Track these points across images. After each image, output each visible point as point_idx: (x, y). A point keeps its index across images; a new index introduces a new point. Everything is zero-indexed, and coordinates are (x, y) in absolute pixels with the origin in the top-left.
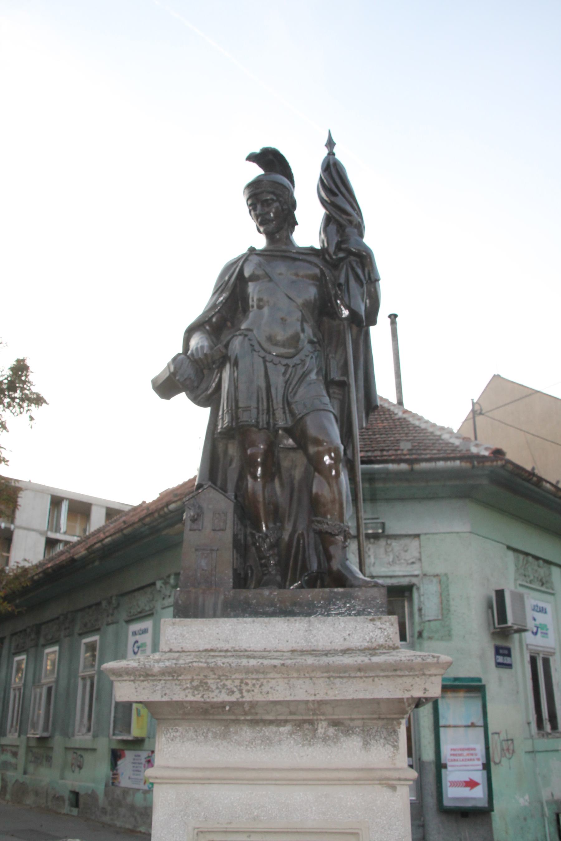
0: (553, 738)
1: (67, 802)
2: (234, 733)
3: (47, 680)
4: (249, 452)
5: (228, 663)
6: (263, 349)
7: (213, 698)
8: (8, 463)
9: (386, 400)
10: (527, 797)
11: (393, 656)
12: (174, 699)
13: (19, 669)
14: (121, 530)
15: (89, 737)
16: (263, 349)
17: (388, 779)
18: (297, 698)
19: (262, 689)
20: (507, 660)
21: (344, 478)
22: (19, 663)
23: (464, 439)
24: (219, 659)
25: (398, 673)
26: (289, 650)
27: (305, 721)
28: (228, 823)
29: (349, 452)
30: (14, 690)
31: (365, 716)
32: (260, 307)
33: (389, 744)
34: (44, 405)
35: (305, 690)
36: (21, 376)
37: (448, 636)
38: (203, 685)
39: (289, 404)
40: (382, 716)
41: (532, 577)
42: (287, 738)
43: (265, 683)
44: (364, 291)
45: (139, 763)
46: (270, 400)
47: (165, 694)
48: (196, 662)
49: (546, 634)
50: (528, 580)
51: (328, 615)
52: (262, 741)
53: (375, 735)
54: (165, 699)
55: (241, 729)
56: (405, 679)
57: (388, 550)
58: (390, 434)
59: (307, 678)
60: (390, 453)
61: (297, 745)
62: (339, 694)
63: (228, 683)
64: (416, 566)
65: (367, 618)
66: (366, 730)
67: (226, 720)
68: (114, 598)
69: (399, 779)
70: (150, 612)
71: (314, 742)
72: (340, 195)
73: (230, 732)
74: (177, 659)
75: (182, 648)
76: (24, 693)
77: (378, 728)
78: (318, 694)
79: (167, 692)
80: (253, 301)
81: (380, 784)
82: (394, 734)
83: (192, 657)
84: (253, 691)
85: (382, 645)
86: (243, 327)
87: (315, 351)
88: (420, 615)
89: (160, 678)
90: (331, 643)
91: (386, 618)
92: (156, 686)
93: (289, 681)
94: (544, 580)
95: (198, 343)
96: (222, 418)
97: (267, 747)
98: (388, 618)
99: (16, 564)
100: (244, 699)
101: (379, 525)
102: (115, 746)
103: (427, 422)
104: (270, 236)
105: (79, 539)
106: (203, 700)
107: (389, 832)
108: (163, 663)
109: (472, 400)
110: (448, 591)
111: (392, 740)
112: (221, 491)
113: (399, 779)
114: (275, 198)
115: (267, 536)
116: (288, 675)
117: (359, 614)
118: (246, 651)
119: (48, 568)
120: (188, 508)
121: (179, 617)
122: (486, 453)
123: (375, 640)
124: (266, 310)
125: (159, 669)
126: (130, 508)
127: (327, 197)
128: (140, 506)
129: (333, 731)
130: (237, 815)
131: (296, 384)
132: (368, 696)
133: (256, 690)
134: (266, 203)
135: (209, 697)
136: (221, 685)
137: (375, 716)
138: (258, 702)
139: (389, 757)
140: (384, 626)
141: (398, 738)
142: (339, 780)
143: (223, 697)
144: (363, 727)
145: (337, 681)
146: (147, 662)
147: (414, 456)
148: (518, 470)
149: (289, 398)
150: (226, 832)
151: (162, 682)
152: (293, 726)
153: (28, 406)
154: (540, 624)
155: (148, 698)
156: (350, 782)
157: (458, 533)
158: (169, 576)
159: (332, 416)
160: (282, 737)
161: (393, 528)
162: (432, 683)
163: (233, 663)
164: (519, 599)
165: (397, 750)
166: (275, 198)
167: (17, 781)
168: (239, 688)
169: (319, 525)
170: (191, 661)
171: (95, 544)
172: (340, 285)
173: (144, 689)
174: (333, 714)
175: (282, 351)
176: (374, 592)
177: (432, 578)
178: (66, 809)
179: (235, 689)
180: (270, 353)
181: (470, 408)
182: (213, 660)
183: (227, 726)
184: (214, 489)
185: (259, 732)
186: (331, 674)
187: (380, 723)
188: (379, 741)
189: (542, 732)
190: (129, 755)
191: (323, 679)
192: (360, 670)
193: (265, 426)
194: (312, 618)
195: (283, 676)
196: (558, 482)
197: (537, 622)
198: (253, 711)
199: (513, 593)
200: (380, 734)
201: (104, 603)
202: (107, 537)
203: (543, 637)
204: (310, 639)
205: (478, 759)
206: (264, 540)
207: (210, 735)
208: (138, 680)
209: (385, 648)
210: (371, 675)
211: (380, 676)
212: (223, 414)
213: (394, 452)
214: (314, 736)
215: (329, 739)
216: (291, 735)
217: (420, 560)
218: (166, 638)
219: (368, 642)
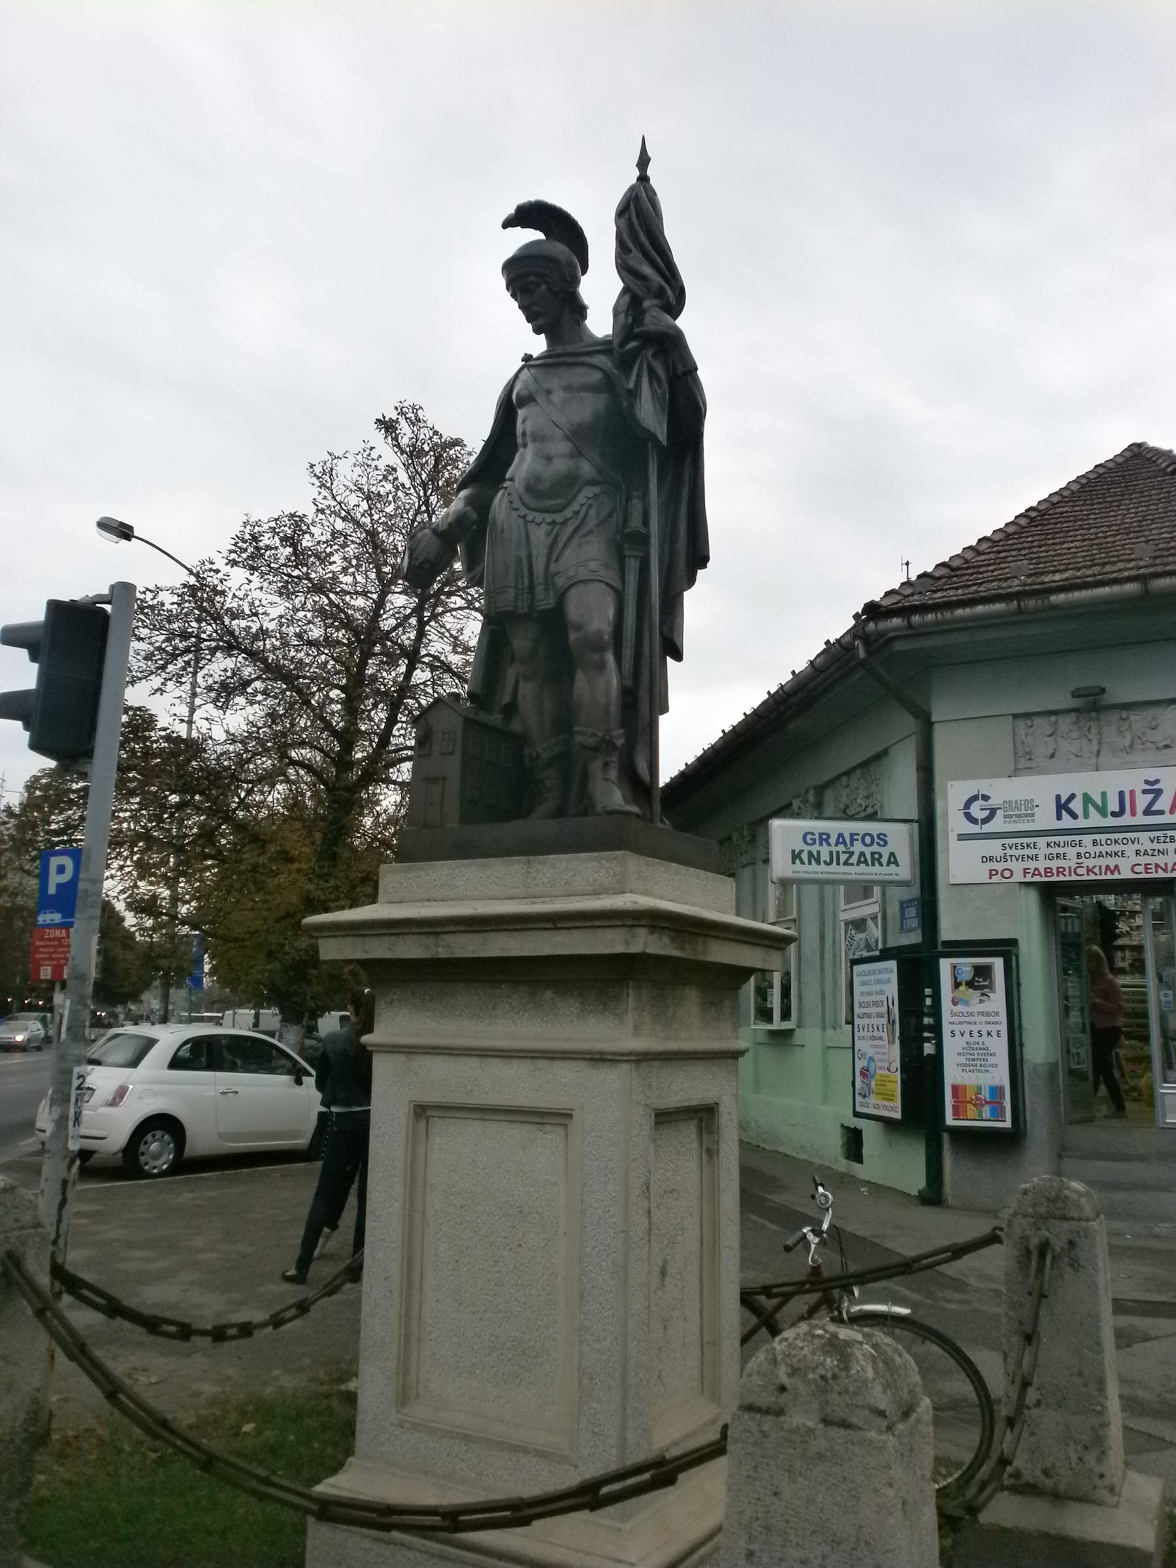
68: (746, 827)
158: (807, 792)
201: (735, 836)
207: (427, 998)
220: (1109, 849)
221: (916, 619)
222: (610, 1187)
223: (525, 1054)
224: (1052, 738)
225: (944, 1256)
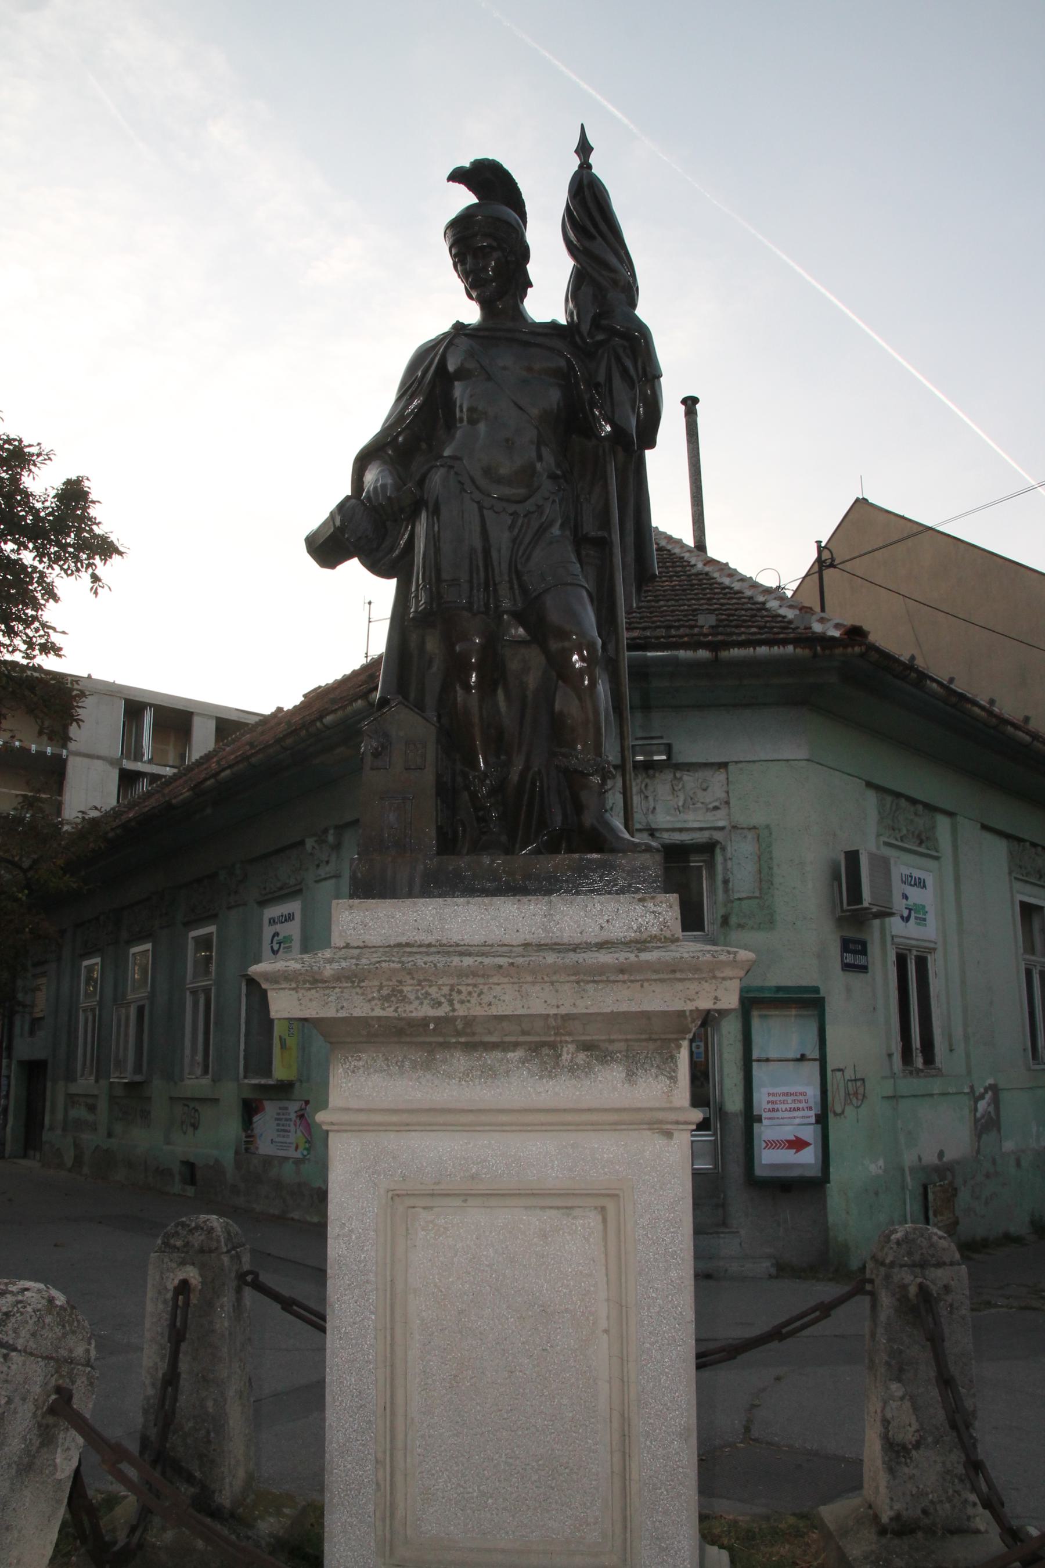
0: (926, 1077)
1: (177, 1178)
2: (441, 1061)
3: (136, 995)
4: (458, 648)
5: (432, 962)
6: (478, 488)
7: (411, 1012)
8: (61, 653)
10: (881, 1163)
11: (672, 951)
12: (355, 1015)
13: (89, 979)
14: (245, 758)
15: (206, 1081)
16: (478, 488)
17: (661, 1122)
18: (532, 1011)
19: (481, 999)
20: (860, 960)
21: (602, 689)
22: (90, 969)
23: (801, 609)
24: (418, 957)
25: (678, 975)
26: (520, 944)
27: (544, 1044)
28: (435, 1183)
29: (611, 653)
30: (85, 1011)
31: (629, 1037)
32: (472, 422)
33: (664, 1075)
34: (115, 557)
36: (76, 508)
37: (769, 922)
38: (397, 995)
39: (519, 575)
40: (654, 1036)
41: (904, 832)
42: (518, 1068)
43: (485, 991)
44: (635, 394)
45: (287, 1120)
46: (490, 569)
47: (342, 1008)
48: (385, 961)
49: (925, 920)
50: (898, 836)
51: (578, 893)
52: (482, 1072)
54: (342, 1014)
56: (687, 984)
57: (676, 788)
58: (683, 599)
59: (546, 982)
60: (682, 631)
61: (532, 1076)
62: (592, 1005)
63: (433, 991)
64: (721, 813)
65: (634, 898)
67: (430, 1043)
69: (677, 1123)
70: (298, 888)
72: (599, 239)
73: (435, 1059)
74: (358, 958)
75: (364, 942)
76: (100, 1015)
80: (461, 411)
81: (649, 1129)
82: (672, 1061)
83: (379, 954)
84: (469, 1001)
85: (656, 936)
86: (446, 453)
87: (559, 490)
88: (726, 890)
89: (334, 985)
90: (581, 933)
91: (662, 897)
92: (329, 996)
94: (924, 837)
95: (377, 480)
96: (417, 597)
98: (665, 897)
99: (80, 815)
100: (456, 1014)
101: (662, 748)
102: (247, 1094)
103: (743, 579)
104: (486, 305)
105: (175, 770)
106: (396, 1015)
107: (661, 1193)
108: (337, 964)
109: (819, 542)
110: (770, 852)
111: (668, 1069)
112: (416, 710)
113: (677, 1123)
114: (495, 244)
115: (485, 775)
116: (519, 979)
117: (622, 891)
118: (458, 945)
119: (130, 820)
120: (369, 735)
121: (359, 897)
122: (837, 634)
123: (646, 929)
124: (482, 427)
125: (332, 972)
126: (257, 719)
127: (578, 240)
128: (274, 715)
129: (584, 1057)
130: (448, 1173)
131: (530, 543)
132: (635, 1008)
134: (481, 253)
135: (405, 1011)
136: (422, 994)
138: (475, 1017)
141: (677, 1066)
142: (592, 1124)
143: (426, 1010)
144: (627, 1050)
145: (590, 987)
146: (315, 962)
147: (720, 638)
148: (886, 661)
149: (519, 567)
150: (432, 1195)
151: (337, 990)
152: (526, 1051)
153: (89, 558)
154: (915, 904)
155: (317, 1013)
156: (607, 1127)
157: (788, 760)
158: (326, 831)
159: (585, 594)
160: (510, 1066)
161: (688, 751)
162: (726, 989)
163: (439, 962)
164: (882, 865)
165: (675, 1083)
166: (495, 244)
167: (97, 1147)
168: (448, 997)
169: (564, 760)
170: (379, 960)
171: (206, 779)
172: (597, 385)
173: (311, 1000)
174: (583, 1034)
175: (508, 491)
176: (646, 858)
177: (745, 831)
178: (177, 1187)
179: (443, 1000)
180: (489, 495)
181: (814, 555)
182: (410, 959)
184: (406, 706)
185: (479, 1059)
186: (582, 977)
187: (651, 1046)
188: (650, 1070)
189: (910, 1068)
190: (270, 1108)
191: (569, 984)
192: (622, 971)
193: (483, 609)
194: (554, 897)
196: (952, 680)
197: (910, 902)
198: (469, 1030)
199: (872, 857)
200: (651, 1061)
202: (223, 770)
203: (919, 924)
205: (810, 1109)
206: (482, 782)
208: (302, 988)
210: (638, 978)
211: (652, 980)
212: (417, 590)
213: (688, 631)
214: (557, 1065)
215: (578, 1068)
216: (523, 1063)
217: (727, 803)
218: (341, 928)
219: (636, 931)
222: (673, 1274)
223: (569, 1118)
225: (813, 1316)
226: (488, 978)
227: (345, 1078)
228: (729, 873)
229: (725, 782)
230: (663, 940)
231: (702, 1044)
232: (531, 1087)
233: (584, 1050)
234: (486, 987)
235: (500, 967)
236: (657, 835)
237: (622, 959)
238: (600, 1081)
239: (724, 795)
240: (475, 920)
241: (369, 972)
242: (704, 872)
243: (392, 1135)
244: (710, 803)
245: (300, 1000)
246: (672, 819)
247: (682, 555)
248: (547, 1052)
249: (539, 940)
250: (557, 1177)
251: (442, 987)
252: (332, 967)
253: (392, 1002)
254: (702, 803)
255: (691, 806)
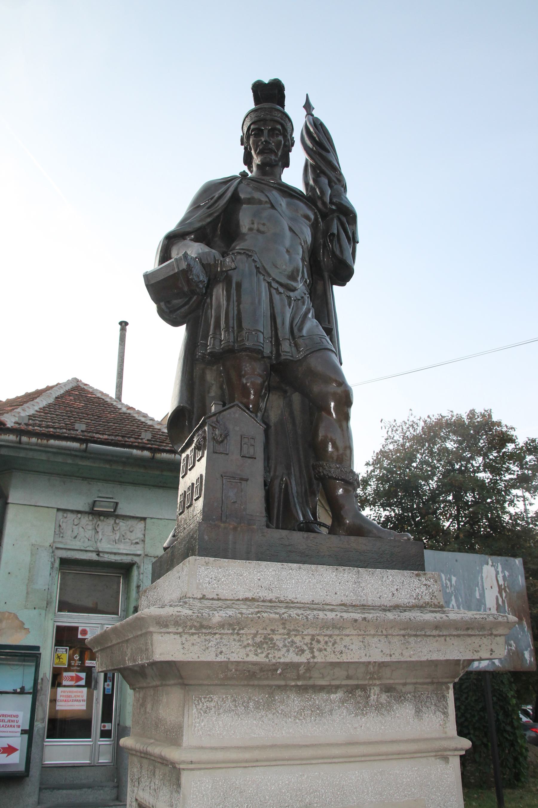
9: (108, 396)
12: (232, 659)
19: (335, 648)
25: (470, 632)
27: (357, 687)
31: (419, 681)
33: (440, 711)
35: (380, 650)
42: (339, 707)
43: (338, 641)
47: (221, 652)
52: (312, 711)
53: (426, 702)
55: (288, 697)
56: (473, 638)
57: (115, 529)
62: (414, 655)
63: (297, 639)
64: (139, 546)
66: (417, 696)
67: (270, 686)
71: (367, 711)
75: (217, 595)
77: (428, 694)
78: (394, 654)
79: (224, 649)
82: (444, 700)
84: (325, 650)
85: (428, 603)
93: (364, 638)
97: (318, 718)
100: (315, 660)
101: (112, 504)
130: (286, 805)
132: (442, 658)
133: (329, 649)
135: (275, 657)
136: (289, 643)
137: (429, 680)
139: (440, 725)
140: (428, 583)
141: (447, 704)
143: (292, 657)
144: (414, 692)
145: (412, 639)
151: (217, 636)
161: (124, 509)
165: (447, 717)
168: (309, 646)
173: (193, 644)
174: (390, 678)
179: (305, 648)
183: (271, 694)
187: (431, 688)
188: (430, 707)
191: (398, 637)
195: (360, 633)
204: (359, 592)
208: (186, 633)
209: (431, 606)
216: (343, 703)
217: (143, 541)
219: (415, 599)
220: (10, 724)
221: (24, 439)
224: (77, 526)
226: (342, 630)
227: (198, 718)
228: (140, 582)
229: (143, 529)
230: (433, 606)
231: (111, 683)
232: (349, 724)
233: (386, 692)
234: (339, 638)
235: (356, 621)
236: (101, 555)
237: (438, 618)
238: (398, 717)
239: (142, 536)
240: (305, 582)
241: (252, 620)
242: (121, 580)
243: (240, 771)
244: (134, 540)
245: (183, 644)
246: (111, 547)
247: (112, 403)
248: (360, 693)
249: (351, 602)
250: (372, 802)
251: (305, 637)
252: (220, 614)
253: (264, 648)
254: (129, 539)
255: (123, 541)
